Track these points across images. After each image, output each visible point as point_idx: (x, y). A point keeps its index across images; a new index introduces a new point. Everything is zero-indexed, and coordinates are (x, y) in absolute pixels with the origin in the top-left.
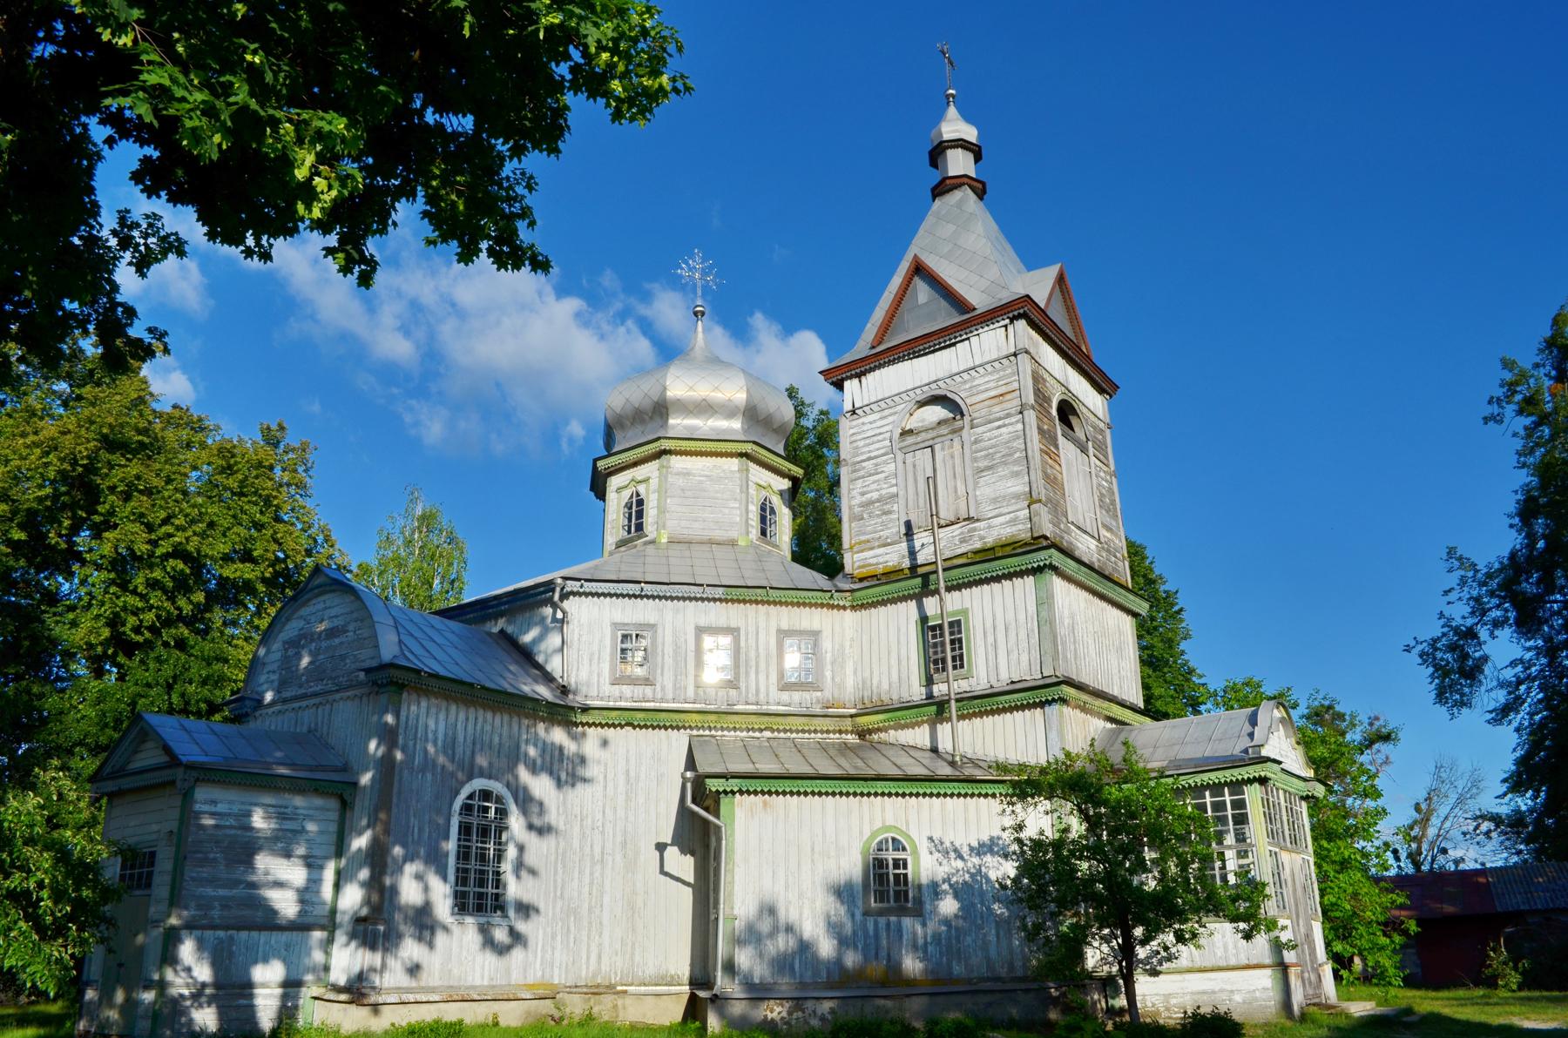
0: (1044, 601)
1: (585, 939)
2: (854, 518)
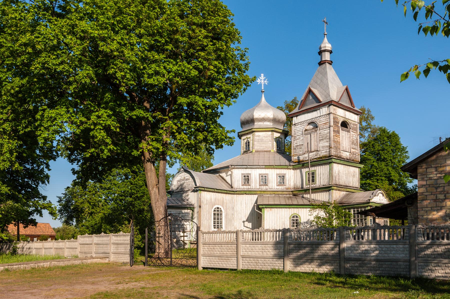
0: (331, 170)
2: (295, 149)
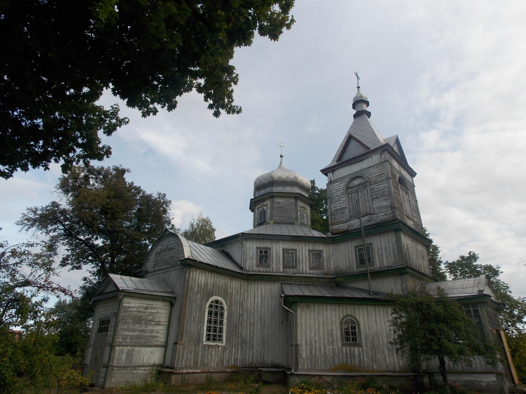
1: (248, 351)
